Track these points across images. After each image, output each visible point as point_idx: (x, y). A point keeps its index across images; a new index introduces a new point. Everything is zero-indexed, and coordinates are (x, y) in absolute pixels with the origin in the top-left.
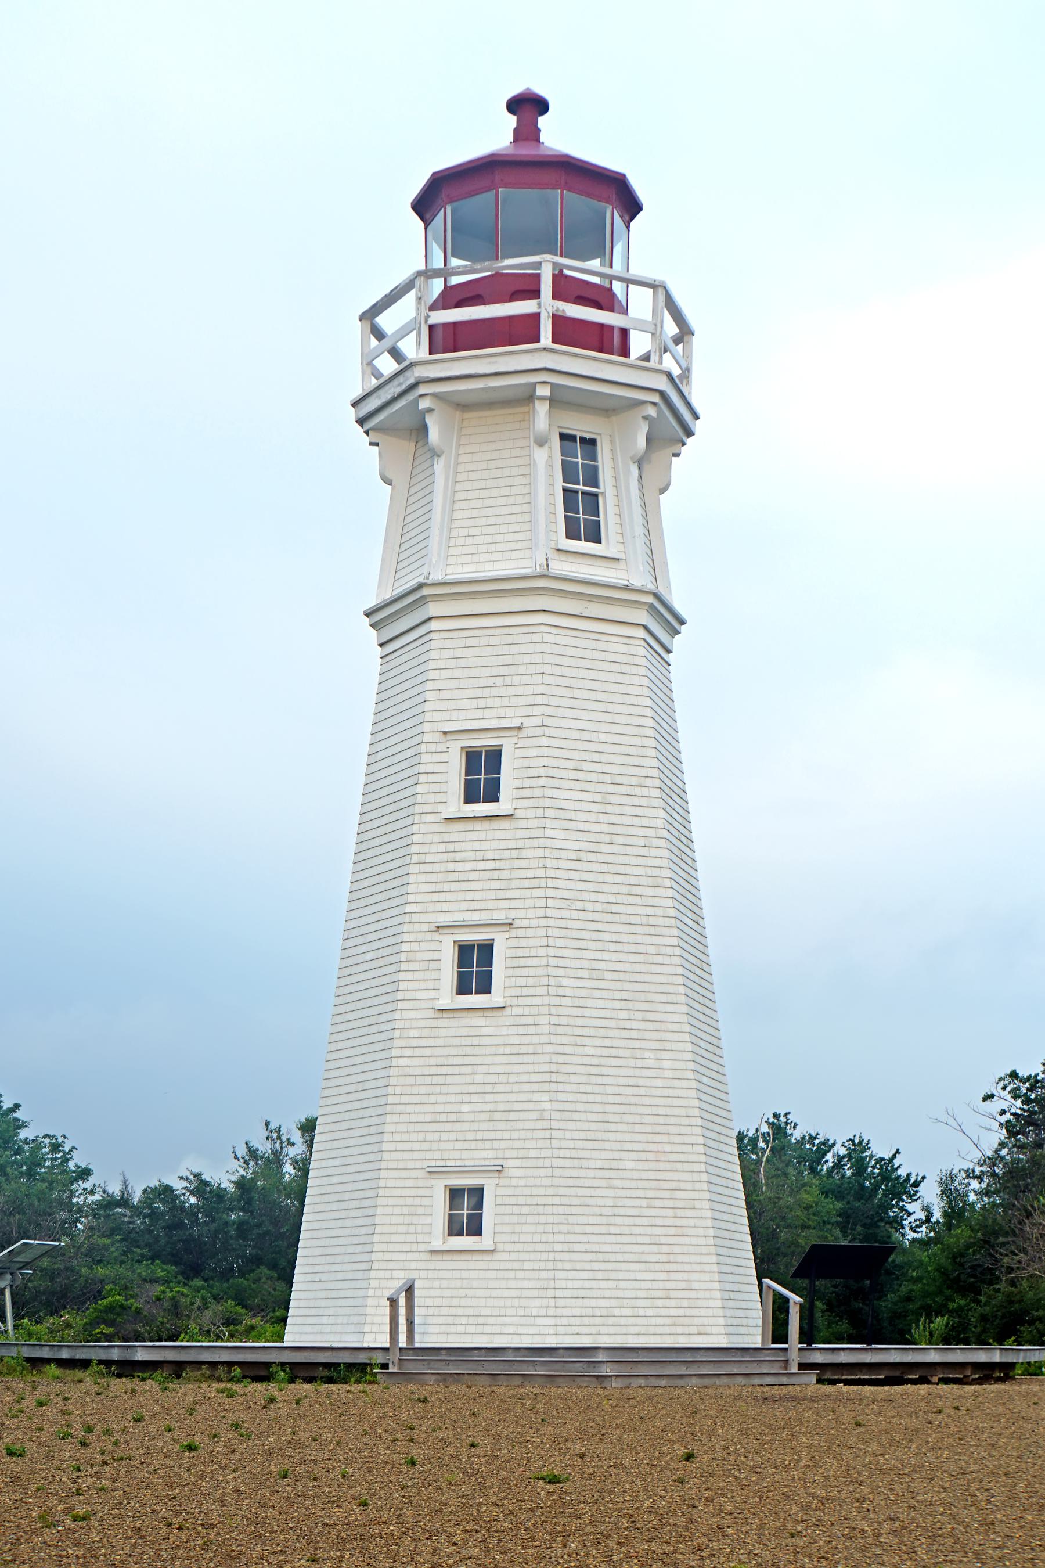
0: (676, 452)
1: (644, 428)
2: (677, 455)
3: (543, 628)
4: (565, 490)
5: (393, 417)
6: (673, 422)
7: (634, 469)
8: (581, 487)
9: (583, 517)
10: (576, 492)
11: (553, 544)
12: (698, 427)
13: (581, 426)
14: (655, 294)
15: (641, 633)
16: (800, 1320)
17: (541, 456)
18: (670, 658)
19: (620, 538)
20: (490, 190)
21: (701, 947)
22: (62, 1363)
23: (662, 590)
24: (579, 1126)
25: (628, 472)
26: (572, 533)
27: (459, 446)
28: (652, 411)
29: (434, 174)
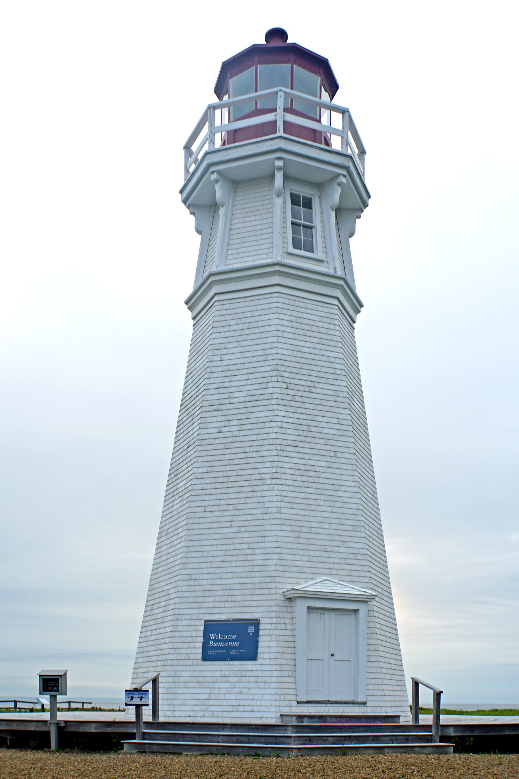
0: (359, 215)
1: (339, 190)
2: (359, 217)
3: (277, 289)
4: (293, 223)
5: (200, 200)
6: (354, 203)
7: (333, 214)
8: (302, 222)
9: (302, 236)
10: (299, 225)
11: (285, 250)
12: (370, 202)
13: (304, 191)
14: (343, 117)
15: (336, 302)
16: (503, 715)
17: (279, 201)
18: (355, 325)
19: (324, 250)
20: (252, 66)
21: (378, 521)
22: (150, 752)
23: (348, 278)
24: (209, 497)
25: (329, 216)
26: (296, 245)
27: (233, 206)
28: (344, 180)
29: (223, 63)
